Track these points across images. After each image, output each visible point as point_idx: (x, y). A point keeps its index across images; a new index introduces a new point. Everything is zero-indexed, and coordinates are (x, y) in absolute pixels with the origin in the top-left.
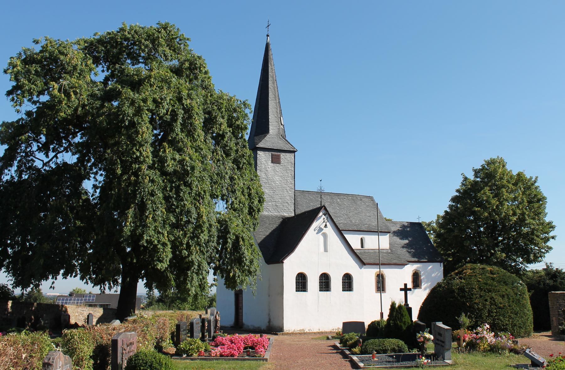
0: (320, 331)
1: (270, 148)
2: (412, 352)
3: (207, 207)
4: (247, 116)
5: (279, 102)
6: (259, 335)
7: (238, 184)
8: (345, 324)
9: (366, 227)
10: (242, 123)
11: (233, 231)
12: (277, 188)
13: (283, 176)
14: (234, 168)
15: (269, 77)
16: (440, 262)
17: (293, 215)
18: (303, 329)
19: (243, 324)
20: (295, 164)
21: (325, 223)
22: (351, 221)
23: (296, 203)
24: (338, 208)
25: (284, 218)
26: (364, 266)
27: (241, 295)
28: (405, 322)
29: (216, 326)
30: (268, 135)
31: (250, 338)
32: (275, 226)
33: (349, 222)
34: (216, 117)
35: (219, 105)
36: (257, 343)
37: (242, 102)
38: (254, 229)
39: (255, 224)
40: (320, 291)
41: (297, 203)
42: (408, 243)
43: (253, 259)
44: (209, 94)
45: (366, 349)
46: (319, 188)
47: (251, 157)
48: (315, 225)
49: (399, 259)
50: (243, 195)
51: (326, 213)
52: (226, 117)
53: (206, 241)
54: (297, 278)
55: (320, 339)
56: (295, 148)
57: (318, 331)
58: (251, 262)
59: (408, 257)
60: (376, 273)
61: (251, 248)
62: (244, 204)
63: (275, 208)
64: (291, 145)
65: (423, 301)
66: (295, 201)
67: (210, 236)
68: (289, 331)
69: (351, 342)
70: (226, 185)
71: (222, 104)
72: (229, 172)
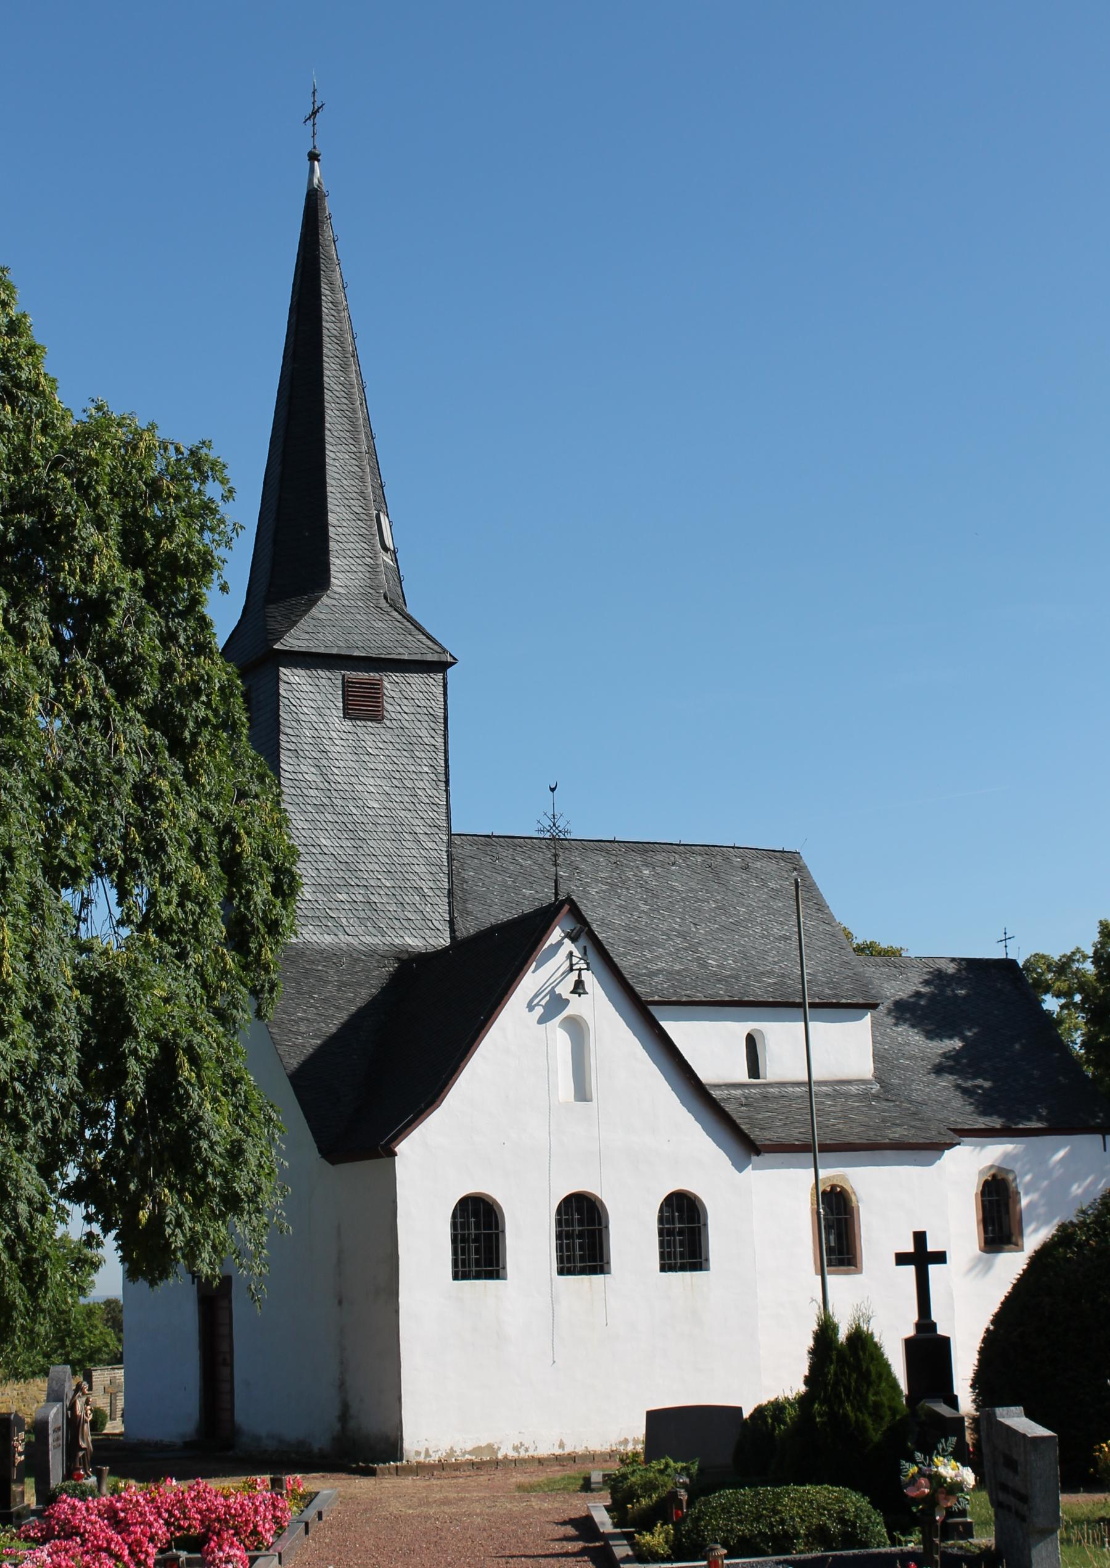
0: (568, 1450)
1: (335, 651)
2: (907, 1542)
3: (21, 923)
4: (214, 512)
5: (372, 452)
6: (267, 1477)
7: (175, 816)
8: (657, 1420)
9: (770, 985)
10: (189, 544)
11: (150, 1023)
12: (370, 827)
13: (397, 775)
14: (153, 747)
15: (326, 339)
17: (445, 941)
18: (490, 1447)
21: (574, 976)
22: (703, 964)
23: (458, 893)
25: (405, 956)
26: (754, 1158)
28: (877, 1406)
29: (71, 1447)
30: (324, 599)
31: (199, 1497)
32: (365, 995)
33: (694, 966)
34: (68, 524)
35: (80, 471)
36: (226, 1521)
37: (186, 453)
38: (259, 1014)
40: (561, 1272)
41: (464, 890)
43: (239, 1141)
44: (39, 423)
45: (699, 1533)
46: (547, 823)
47: (232, 695)
48: (531, 982)
49: (918, 1124)
50: (199, 861)
52: (114, 520)
53: (29, 1070)
54: (459, 1220)
55: (550, 1488)
56: (445, 651)
57: (558, 1452)
58: (235, 1153)
61: (234, 1094)
62: (206, 903)
63: (362, 915)
65: (995, 1308)
66: (451, 882)
67: (49, 1047)
69: (644, 1502)
70: (119, 822)
71: (96, 463)
72: (130, 764)
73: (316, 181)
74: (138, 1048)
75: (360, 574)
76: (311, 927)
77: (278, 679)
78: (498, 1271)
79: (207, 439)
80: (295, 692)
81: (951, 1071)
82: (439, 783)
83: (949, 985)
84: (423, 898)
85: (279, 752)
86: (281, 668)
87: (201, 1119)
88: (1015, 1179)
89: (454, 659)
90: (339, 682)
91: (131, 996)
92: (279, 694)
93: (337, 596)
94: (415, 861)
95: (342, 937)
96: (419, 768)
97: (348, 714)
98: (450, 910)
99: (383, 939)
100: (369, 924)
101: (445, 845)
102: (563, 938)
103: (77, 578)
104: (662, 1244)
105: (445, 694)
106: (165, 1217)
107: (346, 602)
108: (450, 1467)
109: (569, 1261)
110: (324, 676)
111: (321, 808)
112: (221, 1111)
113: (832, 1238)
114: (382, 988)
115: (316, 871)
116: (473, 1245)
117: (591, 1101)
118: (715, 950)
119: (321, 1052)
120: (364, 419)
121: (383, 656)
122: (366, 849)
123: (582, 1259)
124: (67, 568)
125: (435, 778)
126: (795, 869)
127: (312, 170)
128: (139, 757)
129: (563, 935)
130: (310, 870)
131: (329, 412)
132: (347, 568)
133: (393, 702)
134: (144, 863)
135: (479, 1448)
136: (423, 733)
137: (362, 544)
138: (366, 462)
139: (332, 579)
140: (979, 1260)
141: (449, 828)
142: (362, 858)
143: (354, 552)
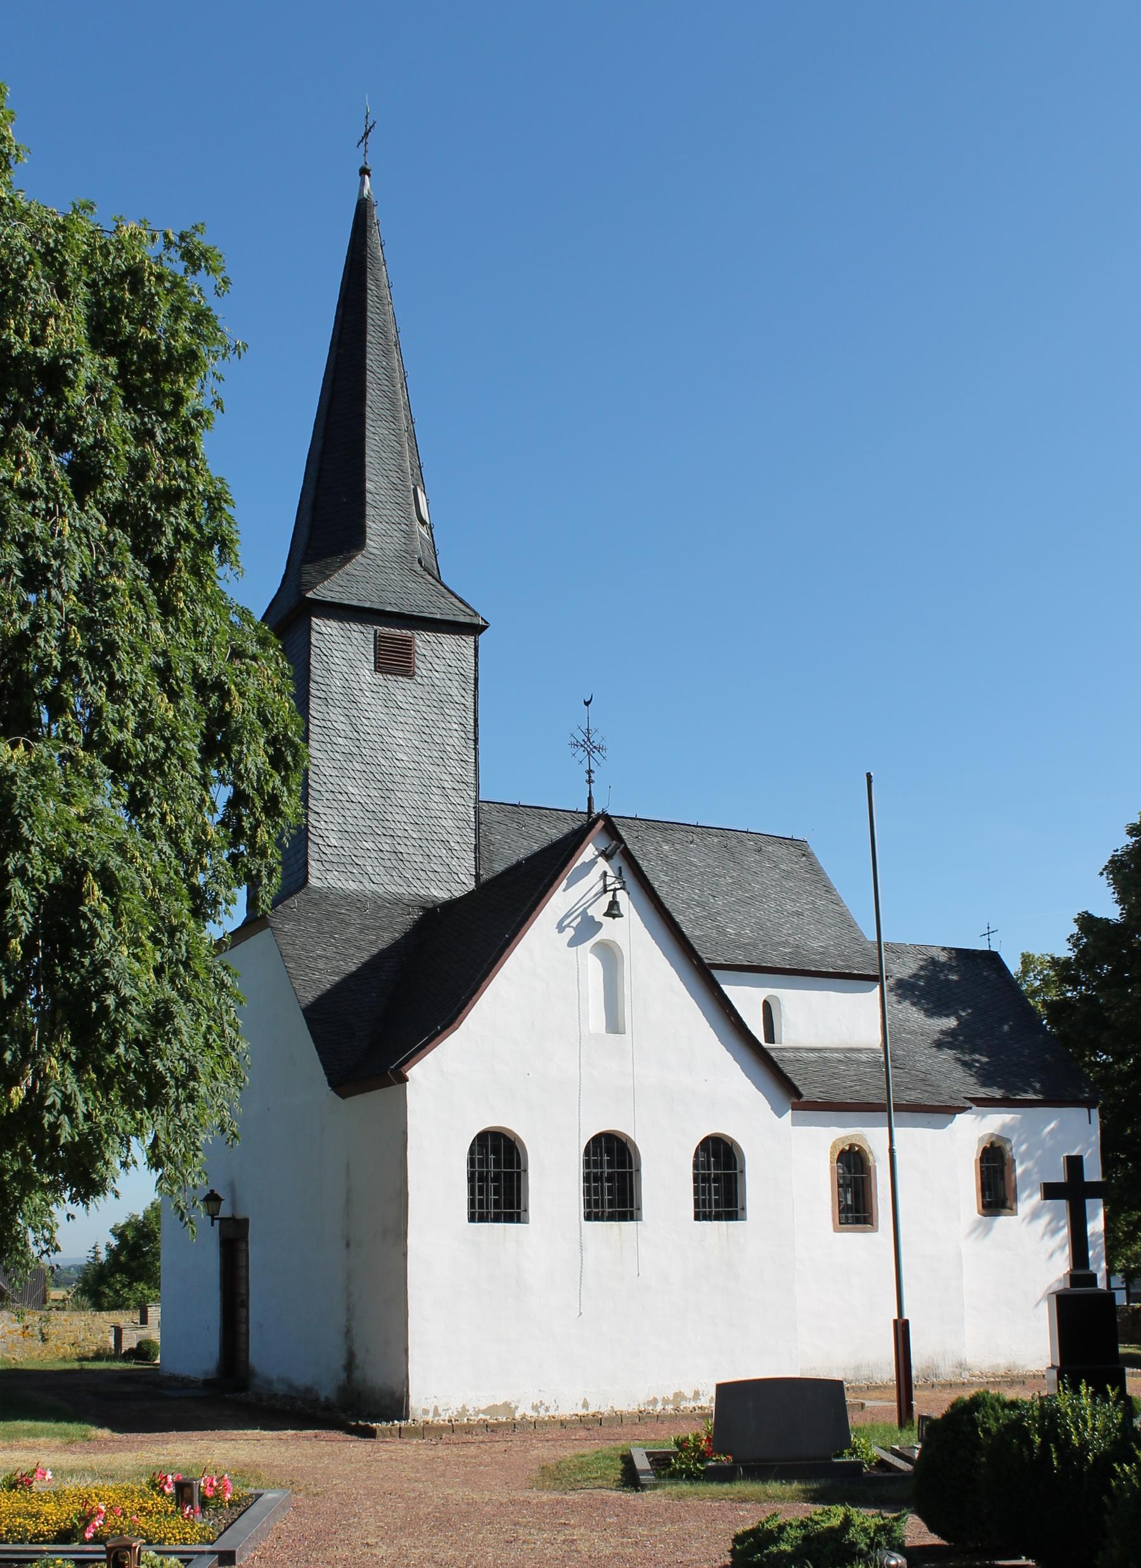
1: (367, 605)
8: (724, 1390)
9: (786, 954)
12: (398, 779)
13: (427, 730)
15: (370, 328)
16: (1089, 1104)
18: (506, 1405)
19: (249, 1373)
20: (476, 680)
21: (608, 897)
22: (721, 931)
24: (666, 879)
25: (430, 906)
27: (243, 1246)
32: (387, 939)
33: (714, 934)
39: (258, 876)
40: (588, 1217)
42: (954, 1030)
43: (166, 1001)
51: (616, 848)
56: (476, 614)
57: (582, 1412)
58: (161, 1017)
59: (961, 1082)
60: (834, 1146)
62: (172, 737)
63: (388, 864)
64: (461, 601)
66: (477, 837)
68: (436, 1413)
73: (366, 192)
74: (28, 866)
75: (395, 539)
76: (336, 873)
77: (309, 629)
78: (519, 1214)
79: (198, 222)
80: (326, 643)
81: (951, 1046)
82: (467, 741)
83: (941, 971)
84: (449, 852)
85: (308, 699)
86: (313, 618)
87: (107, 964)
88: (1011, 1149)
89: (486, 622)
90: (371, 637)
91: (23, 796)
92: (310, 643)
93: (372, 557)
94: (443, 815)
95: (367, 885)
96: (448, 725)
97: (380, 667)
98: (476, 865)
99: (409, 889)
100: (394, 874)
101: (472, 801)
102: (597, 857)
103: (27, 339)
104: (696, 1192)
105: (476, 656)
106: (45, 1098)
107: (380, 563)
108: (461, 1430)
109: (597, 1206)
110: (357, 630)
111: (350, 756)
112: (143, 958)
113: (849, 1196)
114: (406, 933)
115: (342, 818)
116: (492, 1185)
117: (624, 1033)
118: (732, 920)
119: (337, 990)
120: (405, 403)
121: (415, 614)
122: (393, 800)
123: (611, 1204)
124: (13, 326)
125: (464, 736)
126: (804, 855)
127: (363, 183)
128: (91, 551)
129: (596, 853)
130: (336, 817)
131: (371, 391)
132: (383, 532)
133: (424, 660)
134: (87, 668)
135: (495, 1406)
136: (454, 692)
137: (399, 512)
138: (405, 439)
139: (367, 541)
140: (978, 1224)
141: (477, 796)
142: (389, 808)
143: (391, 518)
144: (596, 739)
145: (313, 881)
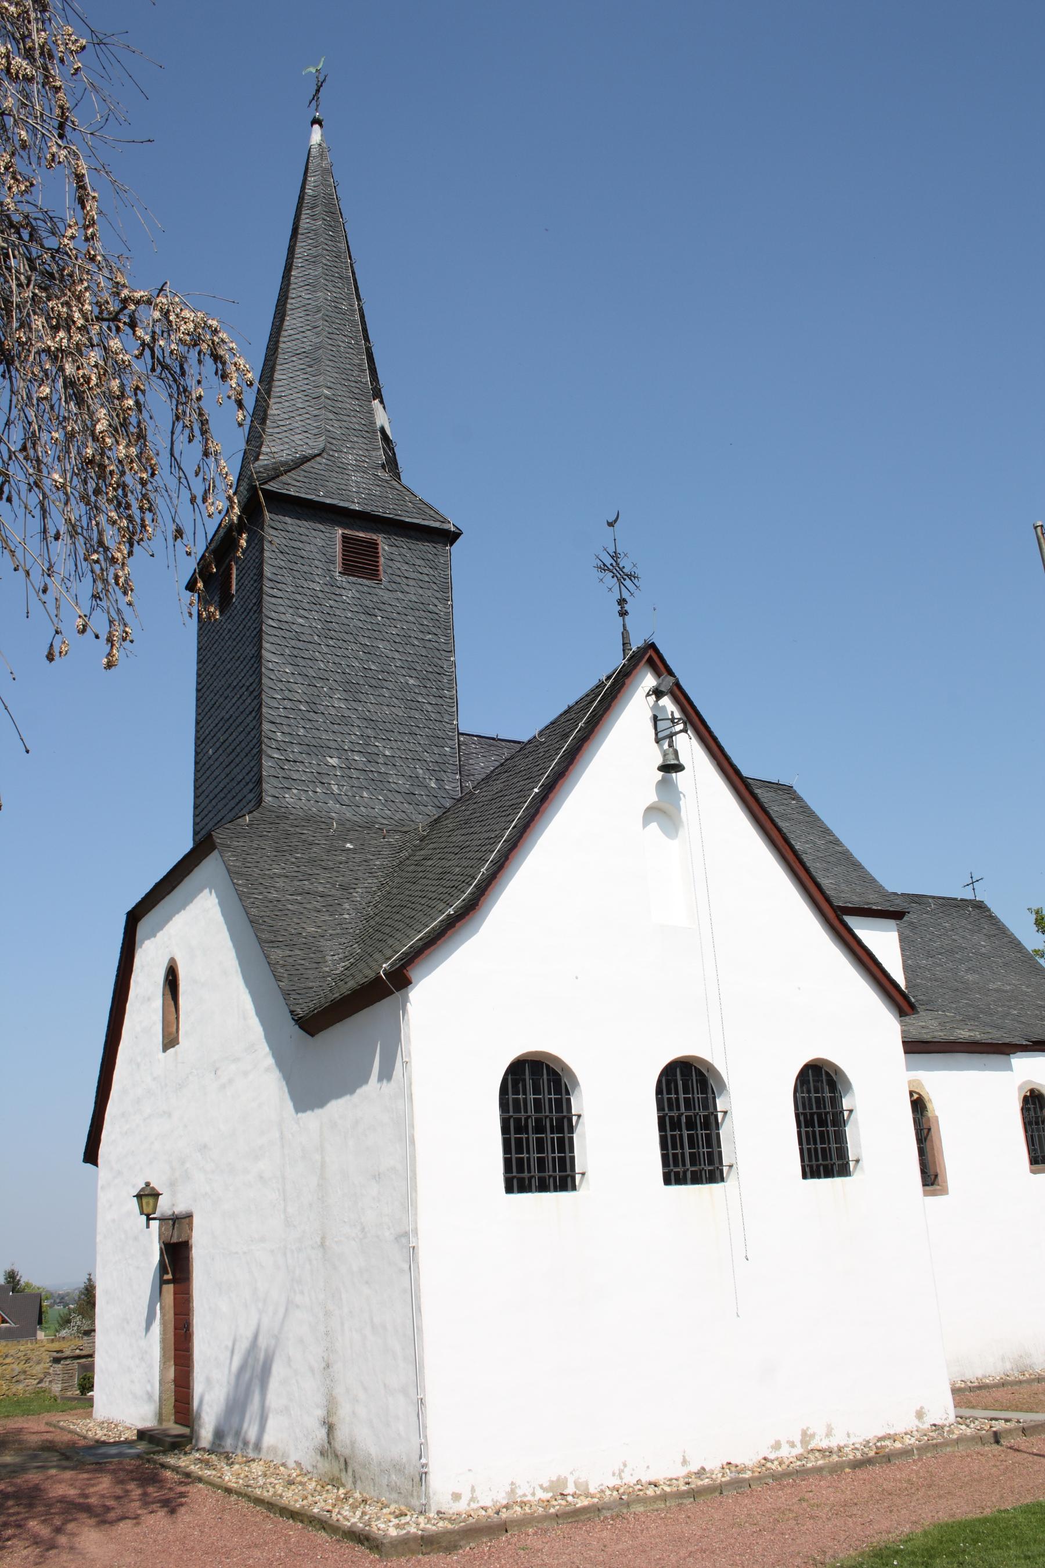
144: (626, 564)
145: (268, 799)
